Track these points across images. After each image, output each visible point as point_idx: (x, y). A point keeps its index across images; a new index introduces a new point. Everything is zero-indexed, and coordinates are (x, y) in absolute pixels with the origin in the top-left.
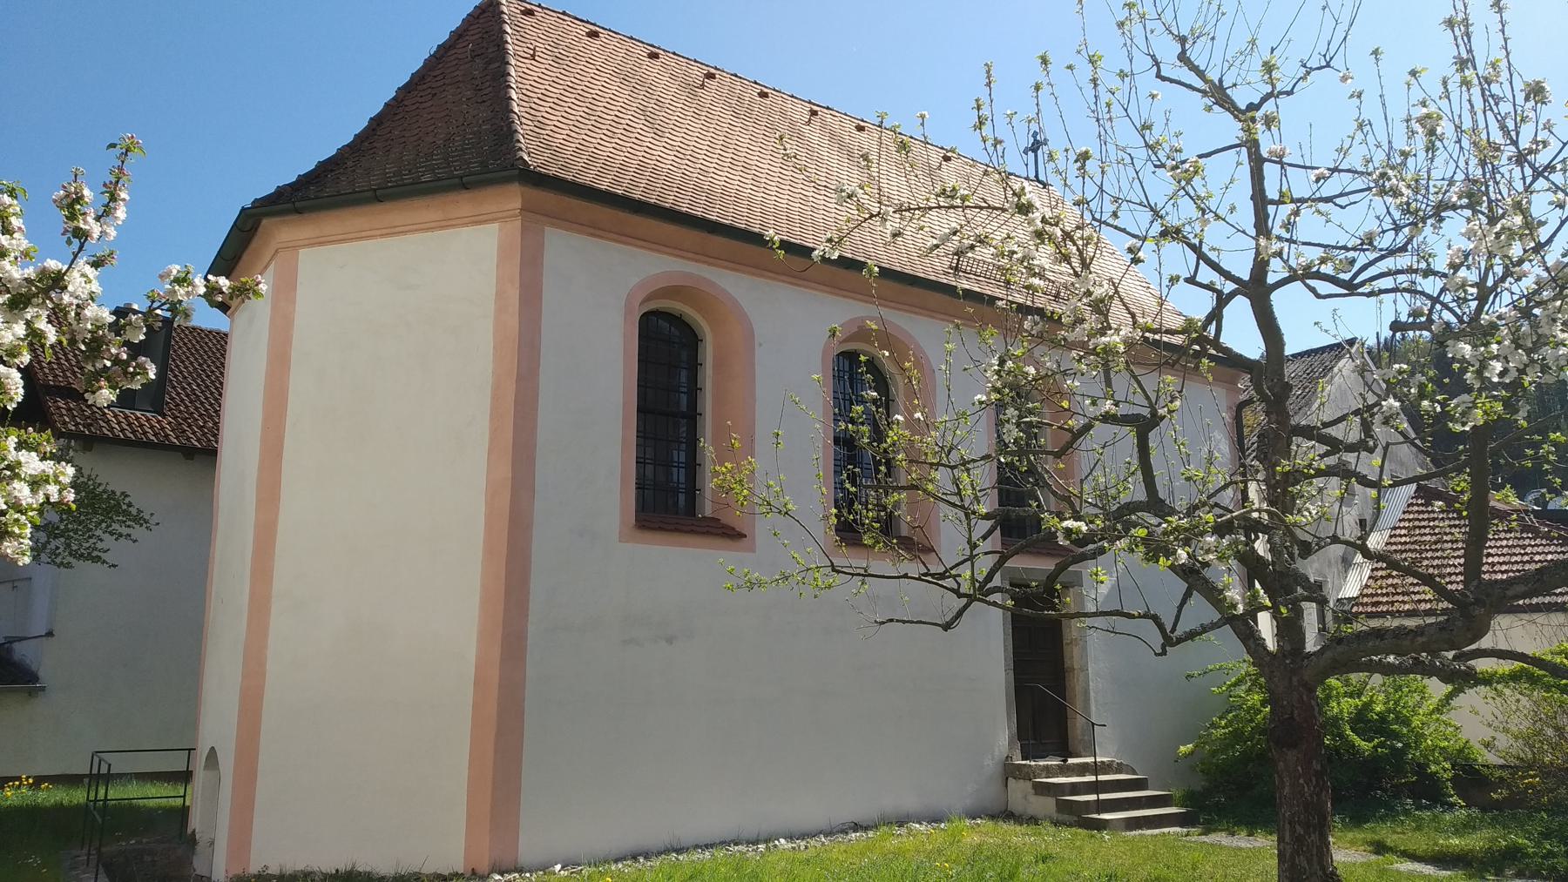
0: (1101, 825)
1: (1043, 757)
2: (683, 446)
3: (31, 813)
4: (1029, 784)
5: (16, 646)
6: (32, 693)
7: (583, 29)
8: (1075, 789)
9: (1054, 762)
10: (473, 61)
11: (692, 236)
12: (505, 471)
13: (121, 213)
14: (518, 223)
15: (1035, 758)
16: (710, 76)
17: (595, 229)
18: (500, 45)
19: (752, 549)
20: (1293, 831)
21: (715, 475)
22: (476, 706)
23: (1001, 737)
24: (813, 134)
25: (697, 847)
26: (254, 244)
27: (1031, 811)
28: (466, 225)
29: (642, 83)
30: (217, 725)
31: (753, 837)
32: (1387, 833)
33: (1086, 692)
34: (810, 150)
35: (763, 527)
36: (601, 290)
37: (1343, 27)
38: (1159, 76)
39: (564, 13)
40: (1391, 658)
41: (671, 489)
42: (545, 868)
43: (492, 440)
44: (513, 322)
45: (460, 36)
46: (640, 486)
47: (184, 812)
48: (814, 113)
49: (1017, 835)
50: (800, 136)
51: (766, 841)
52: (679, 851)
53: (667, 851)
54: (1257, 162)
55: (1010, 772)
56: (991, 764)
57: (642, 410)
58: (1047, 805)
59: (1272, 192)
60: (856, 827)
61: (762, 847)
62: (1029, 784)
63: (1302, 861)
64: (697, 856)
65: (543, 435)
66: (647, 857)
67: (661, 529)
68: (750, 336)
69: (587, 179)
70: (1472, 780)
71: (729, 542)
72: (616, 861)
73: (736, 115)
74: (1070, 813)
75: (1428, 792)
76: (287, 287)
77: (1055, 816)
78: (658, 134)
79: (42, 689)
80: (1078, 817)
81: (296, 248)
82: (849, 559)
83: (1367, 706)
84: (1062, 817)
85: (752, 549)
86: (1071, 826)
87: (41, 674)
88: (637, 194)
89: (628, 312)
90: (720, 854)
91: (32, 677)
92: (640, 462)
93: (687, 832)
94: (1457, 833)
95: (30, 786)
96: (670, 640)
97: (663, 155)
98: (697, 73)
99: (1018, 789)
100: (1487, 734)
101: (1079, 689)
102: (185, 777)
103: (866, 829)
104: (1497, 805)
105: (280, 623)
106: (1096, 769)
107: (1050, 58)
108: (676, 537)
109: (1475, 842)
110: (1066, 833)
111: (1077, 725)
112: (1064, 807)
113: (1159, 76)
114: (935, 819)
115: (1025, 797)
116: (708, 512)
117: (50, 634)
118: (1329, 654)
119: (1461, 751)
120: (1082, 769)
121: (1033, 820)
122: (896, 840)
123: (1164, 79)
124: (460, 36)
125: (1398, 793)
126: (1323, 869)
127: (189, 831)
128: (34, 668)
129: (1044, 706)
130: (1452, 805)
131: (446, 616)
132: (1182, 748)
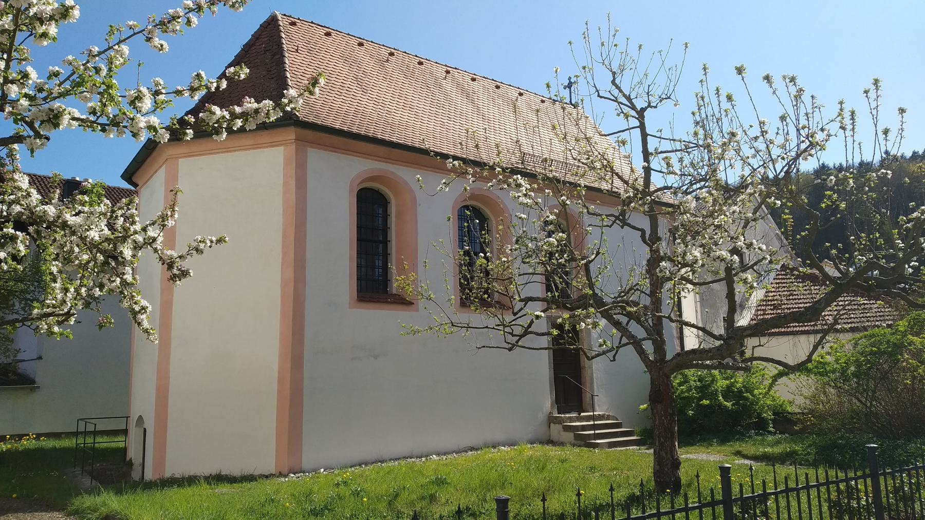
0: (596, 446)
1: (569, 413)
2: (381, 258)
3: (40, 451)
4: (561, 426)
5: (20, 365)
6: (32, 390)
7: (323, 31)
8: (584, 428)
9: (574, 415)
10: (264, 54)
11: (383, 150)
12: (290, 273)
13: (176, 216)
14: (294, 147)
15: (564, 413)
16: (392, 54)
17: (334, 148)
18: (282, 49)
19: (417, 311)
20: (660, 440)
21: (397, 282)
22: (279, 392)
23: (547, 402)
24: (448, 85)
25: (390, 460)
26: (154, 154)
27: (562, 440)
28: (267, 147)
29: (355, 61)
30: (142, 402)
31: (419, 454)
32: (737, 446)
33: (592, 379)
34: (446, 95)
35: (422, 303)
36: (336, 182)
37: (672, 84)
38: (599, 96)
39: (312, 23)
40: (708, 362)
41: (374, 281)
42: (316, 470)
43: (283, 259)
44: (292, 197)
45: (257, 38)
46: (359, 279)
47: (124, 450)
48: (448, 72)
49: (553, 452)
50: (441, 86)
51: (426, 456)
52: (382, 462)
53: (376, 462)
54: (644, 136)
55: (551, 420)
56: (542, 416)
57: (359, 240)
58: (570, 436)
59: (651, 149)
60: (472, 449)
61: (424, 459)
62: (561, 426)
63: (663, 453)
64: (391, 464)
65: (309, 256)
66: (366, 464)
67: (370, 301)
68: (414, 199)
69: (329, 122)
70: (784, 420)
71: (405, 307)
72: (351, 467)
73: (406, 77)
74: (581, 440)
75: (761, 426)
76: (173, 177)
77: (573, 441)
78: (364, 92)
79: (38, 387)
80: (584, 442)
81: (177, 158)
82: (464, 317)
83: (732, 385)
84: (576, 442)
85: (417, 311)
86: (580, 446)
87: (36, 380)
88: (355, 130)
89: (351, 191)
90: (403, 462)
91: (33, 382)
92: (359, 266)
93: (386, 452)
94: (772, 447)
95: (34, 439)
96: (376, 357)
97: (368, 105)
98: (385, 53)
99: (556, 428)
100: (791, 397)
101: (588, 378)
102: (125, 432)
103: (477, 450)
104: (797, 432)
105: (176, 353)
106: (593, 418)
107: (550, 84)
108: (377, 305)
109: (777, 450)
110: (577, 450)
111: (587, 398)
112: (578, 437)
113: (599, 96)
114: (512, 444)
115: (559, 433)
116: (394, 292)
117: (40, 358)
118: (674, 361)
119: (781, 406)
120: (588, 418)
121: (562, 444)
122: (492, 454)
123: (601, 97)
124: (257, 38)
125: (748, 427)
126: (673, 457)
127: (128, 459)
128: (32, 376)
129: (569, 386)
130: (770, 433)
131: (261, 347)
132: (642, 407)
